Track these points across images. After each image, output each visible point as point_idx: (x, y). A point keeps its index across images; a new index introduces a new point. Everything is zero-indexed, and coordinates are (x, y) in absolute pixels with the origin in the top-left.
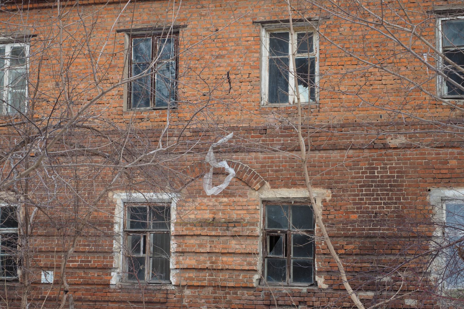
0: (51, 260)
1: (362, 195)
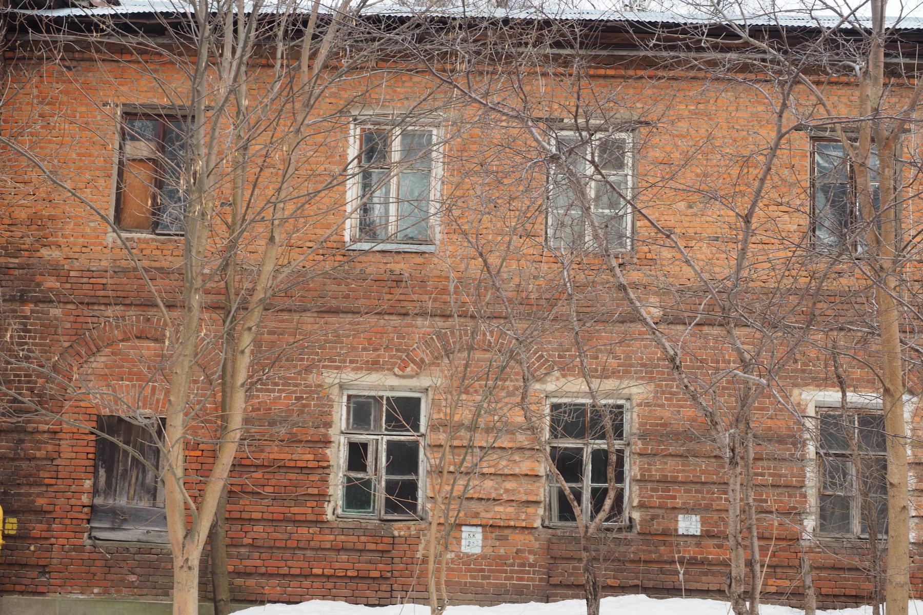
0: (694, 496)
1: (34, 344)
